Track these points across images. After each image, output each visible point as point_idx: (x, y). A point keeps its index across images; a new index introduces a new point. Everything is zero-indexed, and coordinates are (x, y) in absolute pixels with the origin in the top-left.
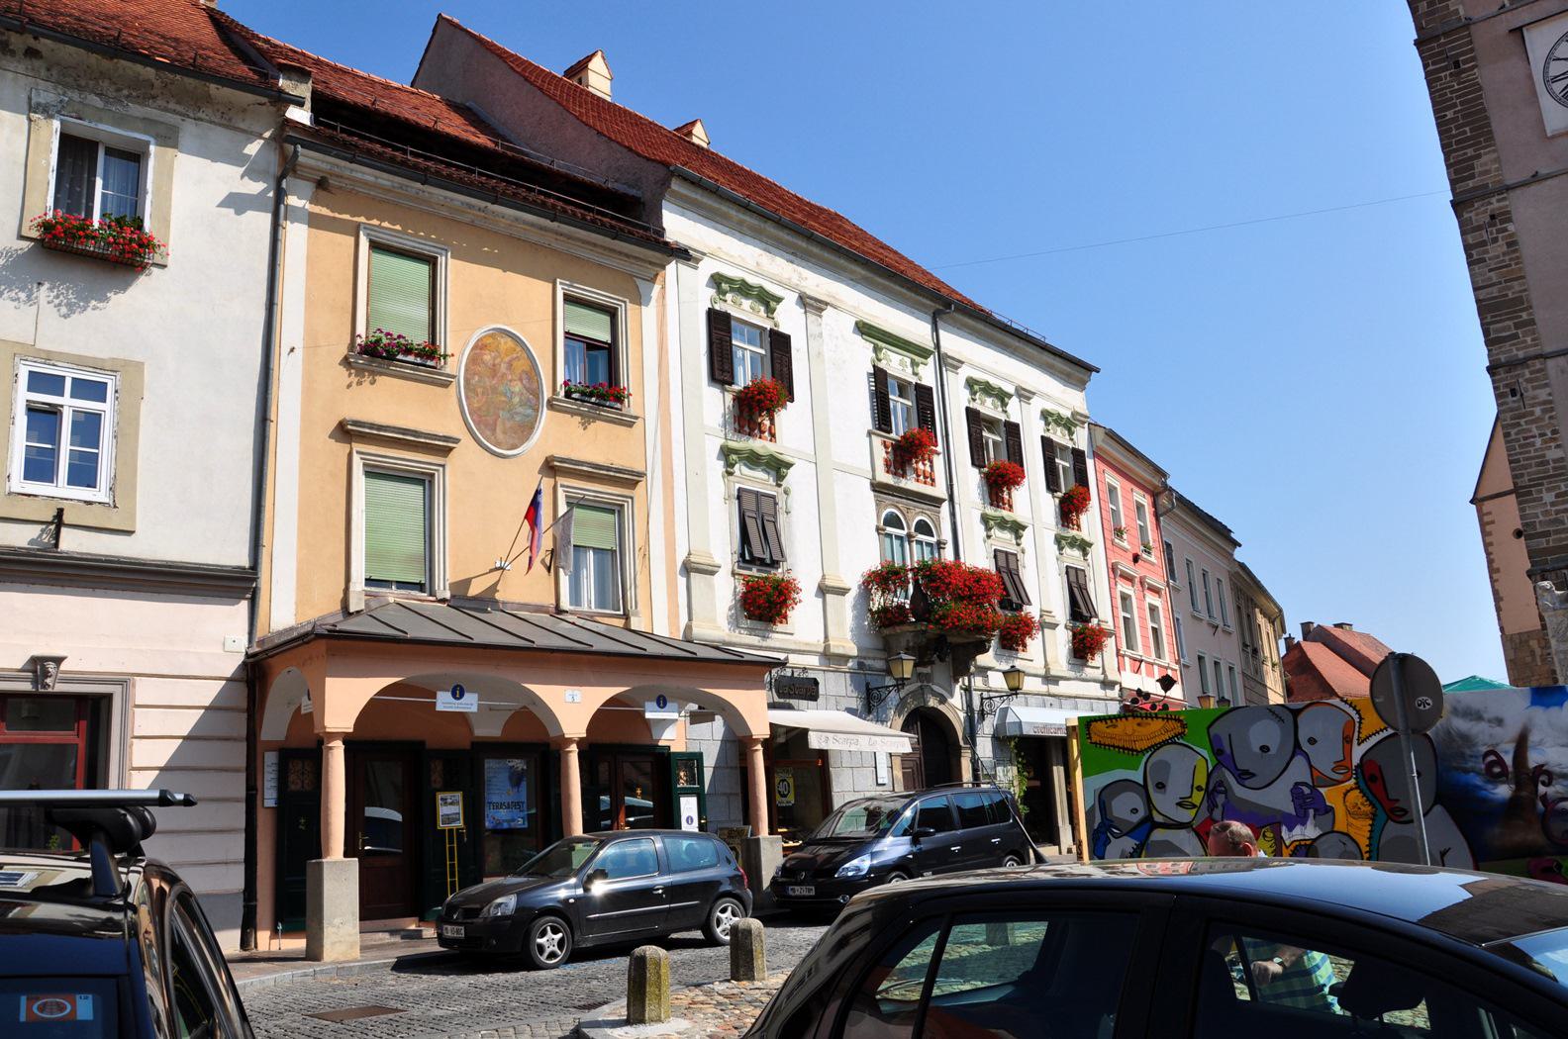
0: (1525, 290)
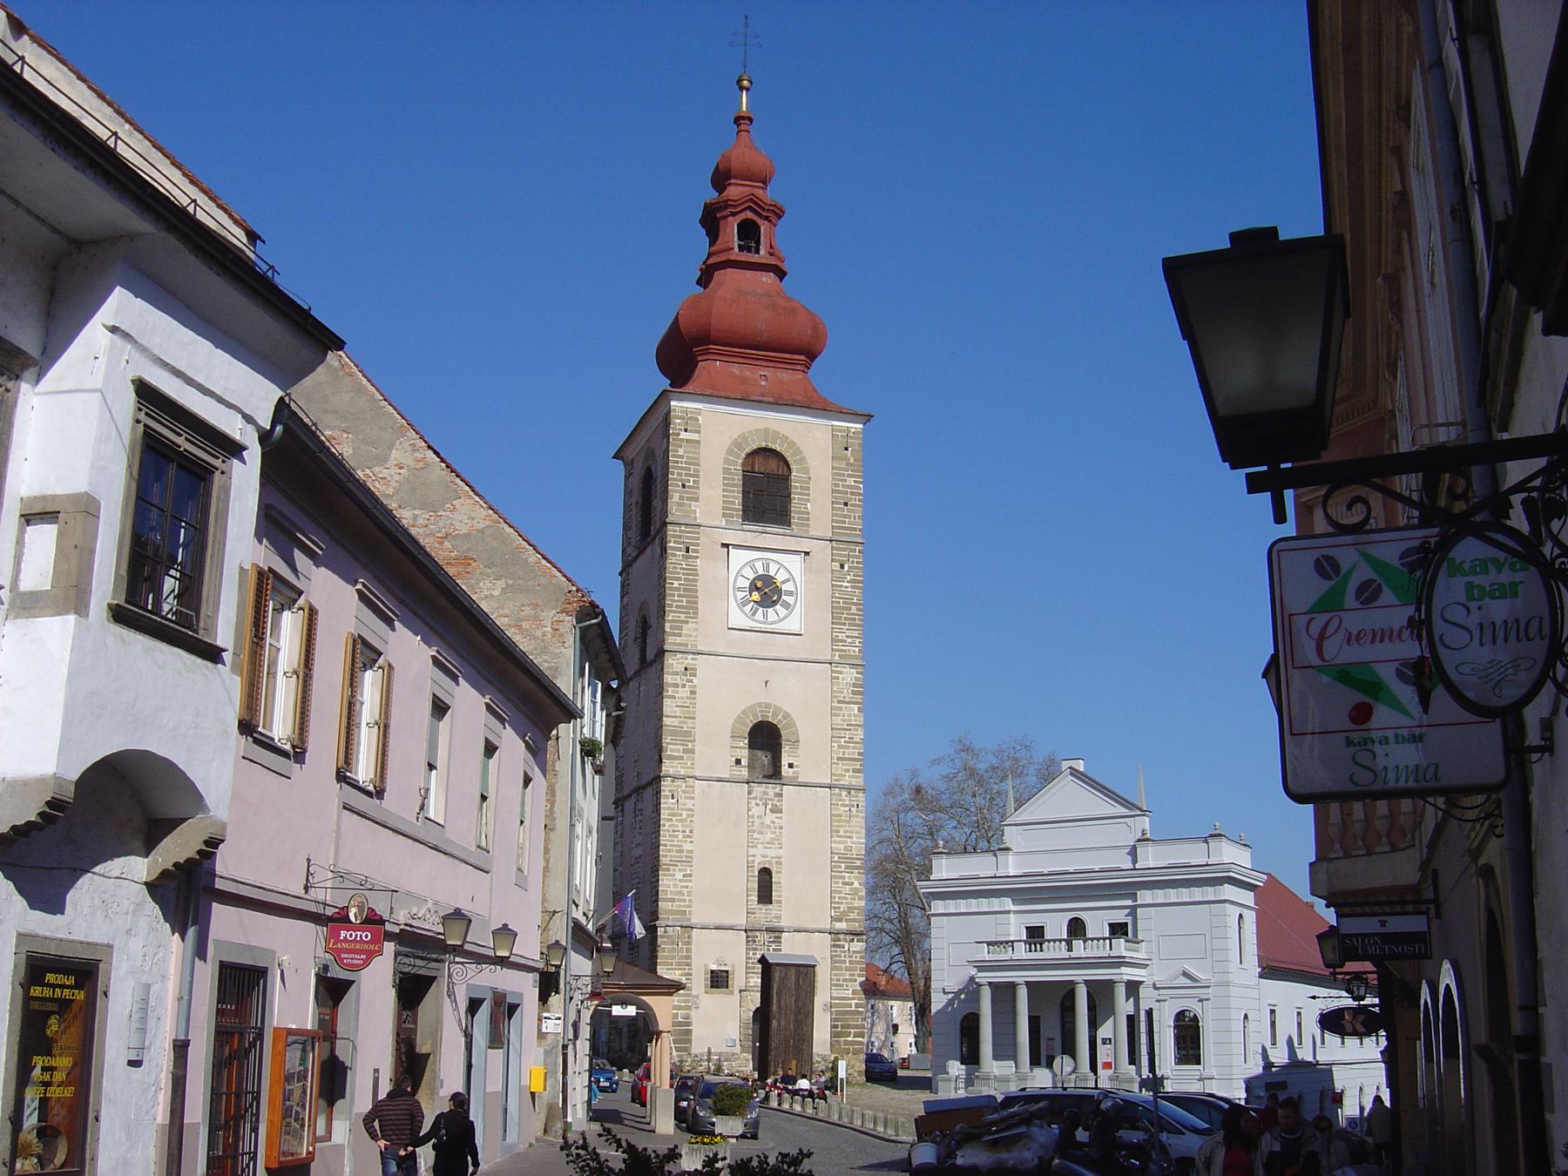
0: (694, 728)
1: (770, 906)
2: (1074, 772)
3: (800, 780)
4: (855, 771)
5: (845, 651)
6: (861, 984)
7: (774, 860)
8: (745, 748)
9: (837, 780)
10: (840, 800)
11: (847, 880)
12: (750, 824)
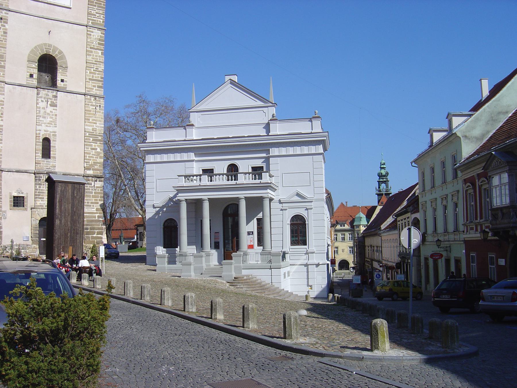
0: (5, 53)
1: (49, 160)
2: (232, 82)
3: (67, 89)
4: (99, 87)
5: (95, 20)
6: (100, 205)
7: (52, 133)
8: (36, 68)
9: (88, 91)
10: (90, 102)
11: (93, 147)
12: (38, 112)
